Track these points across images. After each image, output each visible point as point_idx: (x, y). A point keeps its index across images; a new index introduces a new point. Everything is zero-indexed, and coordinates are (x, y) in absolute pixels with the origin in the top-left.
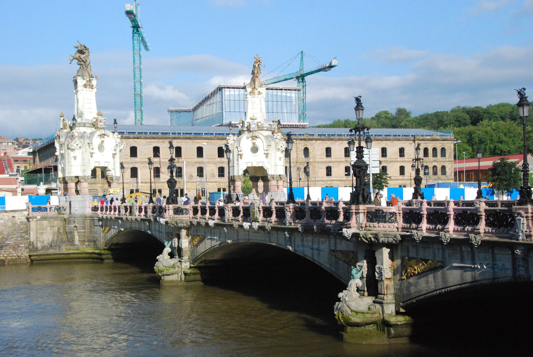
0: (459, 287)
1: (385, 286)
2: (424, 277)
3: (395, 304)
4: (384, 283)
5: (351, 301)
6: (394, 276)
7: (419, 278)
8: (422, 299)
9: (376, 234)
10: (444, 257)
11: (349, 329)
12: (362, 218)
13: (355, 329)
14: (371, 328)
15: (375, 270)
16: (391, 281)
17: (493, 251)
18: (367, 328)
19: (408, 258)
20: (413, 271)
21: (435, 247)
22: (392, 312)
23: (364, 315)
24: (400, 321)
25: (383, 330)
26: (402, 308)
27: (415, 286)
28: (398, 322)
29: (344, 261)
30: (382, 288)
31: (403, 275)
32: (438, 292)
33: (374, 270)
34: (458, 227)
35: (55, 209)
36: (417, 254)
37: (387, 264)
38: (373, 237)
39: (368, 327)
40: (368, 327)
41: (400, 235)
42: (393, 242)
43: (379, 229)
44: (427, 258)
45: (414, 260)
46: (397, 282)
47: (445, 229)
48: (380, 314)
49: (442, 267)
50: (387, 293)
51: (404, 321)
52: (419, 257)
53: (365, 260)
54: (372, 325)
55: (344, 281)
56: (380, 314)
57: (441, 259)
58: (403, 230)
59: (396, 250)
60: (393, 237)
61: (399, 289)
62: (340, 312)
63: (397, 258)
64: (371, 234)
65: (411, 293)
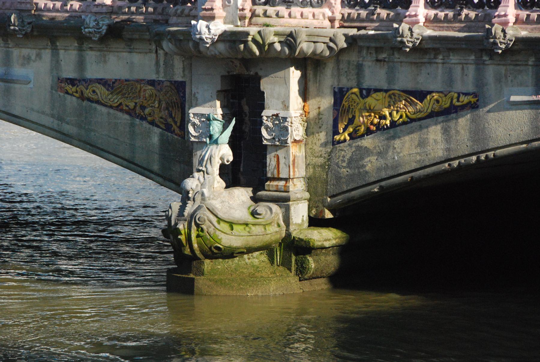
0: (526, 148)
1: (291, 159)
2: (412, 132)
3: (309, 200)
4: (288, 152)
5: (213, 199)
6: (306, 135)
7: (394, 137)
8: (405, 184)
9: (291, 35)
10: (480, 82)
11: (208, 264)
13: (221, 264)
14: (257, 260)
15: (261, 123)
16: (300, 146)
18: (247, 260)
19: (361, 90)
20: (376, 121)
21: (453, 61)
22: (303, 220)
23: (247, 229)
24: (329, 240)
25: (286, 264)
26: (329, 210)
27: (381, 154)
28: (326, 240)
30: (282, 165)
31: (341, 131)
32: (455, 164)
34: (528, 13)
36: (391, 79)
37: (296, 108)
38: (280, 42)
39: (249, 259)
40: (249, 259)
41: (345, 35)
42: (324, 54)
43: (293, 21)
44: (424, 88)
45: (380, 95)
46: (317, 148)
47: (407, 19)
48: (279, 225)
49: (474, 106)
50: (294, 175)
51: (335, 239)
52: (396, 88)
53: (218, 100)
54: (257, 253)
56: (279, 225)
57: (471, 88)
58: (346, 24)
59: (315, 75)
60: (327, 40)
61: (322, 166)
62: (193, 224)
63: (320, 93)
64: (277, 34)
65: (367, 172)
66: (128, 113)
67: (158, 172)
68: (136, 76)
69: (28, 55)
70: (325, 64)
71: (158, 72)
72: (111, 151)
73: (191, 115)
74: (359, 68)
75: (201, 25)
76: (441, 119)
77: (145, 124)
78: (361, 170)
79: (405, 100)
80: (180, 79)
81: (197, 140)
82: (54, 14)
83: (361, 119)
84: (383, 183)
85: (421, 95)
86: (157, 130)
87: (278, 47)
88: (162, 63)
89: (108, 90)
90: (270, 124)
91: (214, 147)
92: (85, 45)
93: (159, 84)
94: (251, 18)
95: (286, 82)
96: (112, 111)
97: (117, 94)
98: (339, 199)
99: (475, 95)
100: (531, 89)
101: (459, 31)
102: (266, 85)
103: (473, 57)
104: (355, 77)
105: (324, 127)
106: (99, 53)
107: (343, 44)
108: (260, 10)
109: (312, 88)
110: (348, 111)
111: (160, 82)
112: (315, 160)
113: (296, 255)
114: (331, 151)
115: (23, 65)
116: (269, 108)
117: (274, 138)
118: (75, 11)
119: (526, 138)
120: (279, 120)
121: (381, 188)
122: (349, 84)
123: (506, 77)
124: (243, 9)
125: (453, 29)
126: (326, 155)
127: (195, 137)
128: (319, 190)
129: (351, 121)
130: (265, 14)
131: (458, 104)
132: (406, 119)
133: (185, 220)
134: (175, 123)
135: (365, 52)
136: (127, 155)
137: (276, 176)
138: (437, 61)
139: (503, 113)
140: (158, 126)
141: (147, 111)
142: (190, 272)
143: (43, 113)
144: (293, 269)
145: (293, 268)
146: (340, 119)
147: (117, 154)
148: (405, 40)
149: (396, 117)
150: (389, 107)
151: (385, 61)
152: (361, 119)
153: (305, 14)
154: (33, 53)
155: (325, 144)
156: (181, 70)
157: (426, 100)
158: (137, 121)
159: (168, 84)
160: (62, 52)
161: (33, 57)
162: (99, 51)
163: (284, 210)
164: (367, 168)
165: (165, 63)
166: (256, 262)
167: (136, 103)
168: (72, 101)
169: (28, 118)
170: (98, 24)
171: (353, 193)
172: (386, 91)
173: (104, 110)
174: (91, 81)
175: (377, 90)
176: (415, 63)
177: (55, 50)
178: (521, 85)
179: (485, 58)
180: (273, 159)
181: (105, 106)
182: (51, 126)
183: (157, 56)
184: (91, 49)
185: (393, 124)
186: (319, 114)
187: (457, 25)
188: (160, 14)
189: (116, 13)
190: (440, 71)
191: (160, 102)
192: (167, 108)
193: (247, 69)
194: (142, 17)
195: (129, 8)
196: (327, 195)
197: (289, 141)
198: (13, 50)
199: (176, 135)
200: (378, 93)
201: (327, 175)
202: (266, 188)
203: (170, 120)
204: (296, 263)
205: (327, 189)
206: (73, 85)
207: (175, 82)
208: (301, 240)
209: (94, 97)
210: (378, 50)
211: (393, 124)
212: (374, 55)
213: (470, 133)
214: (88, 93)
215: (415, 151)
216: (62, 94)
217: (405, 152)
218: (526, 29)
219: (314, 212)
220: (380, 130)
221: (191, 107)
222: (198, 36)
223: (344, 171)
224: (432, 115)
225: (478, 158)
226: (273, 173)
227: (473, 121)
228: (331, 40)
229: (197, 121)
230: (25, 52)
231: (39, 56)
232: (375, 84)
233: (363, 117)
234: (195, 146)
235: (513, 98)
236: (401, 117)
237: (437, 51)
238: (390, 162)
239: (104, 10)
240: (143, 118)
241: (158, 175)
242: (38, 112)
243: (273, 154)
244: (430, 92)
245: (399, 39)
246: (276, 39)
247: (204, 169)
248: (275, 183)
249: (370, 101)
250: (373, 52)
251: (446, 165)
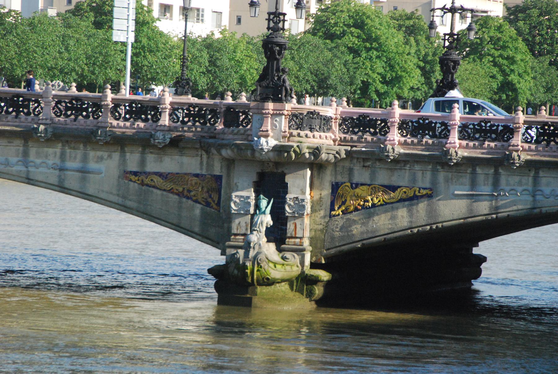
4: (303, 221)
8: (379, 242)
9: (317, 148)
11: (259, 289)
12: (284, 123)
17: (537, 173)
19: (352, 184)
20: (362, 203)
25: (300, 291)
31: (336, 209)
32: (415, 230)
33: (284, 202)
35: (67, 108)
41: (345, 150)
45: (365, 188)
46: (318, 219)
48: (298, 266)
56: (298, 266)
57: (428, 185)
58: (342, 144)
60: (335, 153)
61: (321, 231)
64: (308, 148)
65: (353, 235)
66: (177, 194)
67: (198, 233)
68: (184, 171)
69: (102, 156)
70: (326, 167)
71: (201, 169)
72: (162, 218)
73: (234, 196)
74: (351, 170)
75: (263, 140)
76: (407, 203)
77: (190, 202)
78: (349, 233)
79: (382, 191)
80: (218, 174)
81: (236, 212)
82: (124, 130)
83: (352, 202)
84: (365, 242)
85: (394, 188)
86: (199, 206)
87: (307, 155)
88: (205, 163)
89: (163, 179)
90: (292, 203)
91: (263, 216)
92: (147, 150)
93: (202, 176)
94: (289, 138)
95: (304, 177)
96: (165, 193)
97: (170, 182)
98: (333, 251)
99: (431, 189)
100: (468, 187)
101: (422, 151)
102: (289, 179)
103: (430, 167)
104: (347, 176)
105: (324, 207)
106: (156, 156)
107: (343, 156)
108: (295, 132)
109: (316, 182)
110: (342, 197)
111: (202, 175)
112: (316, 227)
113: (307, 285)
114: (328, 221)
115: (97, 162)
116: (291, 193)
117: (294, 212)
118: (141, 128)
119: (464, 216)
120: (299, 201)
121: (363, 244)
122: (343, 180)
123: (452, 179)
124: (285, 132)
125: (417, 149)
126: (325, 224)
127: (235, 210)
128: (319, 245)
129: (344, 203)
130: (299, 135)
131: (419, 194)
132: (383, 203)
133: (250, 261)
134: (214, 201)
135: (355, 161)
136: (175, 222)
137: (294, 236)
138: (406, 168)
139: (449, 201)
140: (200, 203)
141: (192, 193)
142: (247, 293)
143: (111, 193)
144: (305, 294)
145: (305, 293)
146: (335, 202)
147: (167, 220)
148: (390, 154)
149: (376, 201)
150: (371, 195)
151: (369, 167)
152: (352, 202)
153: (301, 135)
154: (105, 155)
155: (324, 217)
156: (219, 168)
157: (397, 192)
158: (184, 200)
159: (210, 176)
160: (128, 155)
161: (105, 157)
162: (157, 154)
163: (300, 257)
164: (354, 232)
165: (208, 163)
166: (283, 288)
167: (184, 189)
168: (134, 186)
169: (100, 197)
170: (164, 137)
171: (343, 248)
172: (369, 185)
173: (159, 192)
174: (150, 173)
175: (362, 185)
176: (390, 169)
177: (123, 152)
178: (462, 184)
179: (438, 167)
180: (292, 225)
181: (160, 189)
182: (116, 202)
183: (201, 159)
184: (151, 153)
185: (374, 205)
186: (321, 198)
187: (420, 147)
188: (206, 132)
189: (172, 131)
190: (407, 174)
191: (202, 188)
192: (208, 192)
193: (277, 169)
194: (191, 134)
195: (183, 128)
196: (324, 248)
197: (305, 214)
198: (90, 152)
199: (214, 209)
200: (364, 187)
201: (325, 236)
202: (286, 243)
203: (209, 200)
204: (307, 291)
205: (324, 245)
206: (136, 176)
207: (215, 175)
208: (313, 276)
209: (153, 184)
210: (365, 160)
211: (374, 205)
212: (362, 163)
213: (426, 212)
214: (147, 181)
215: (388, 222)
216: (126, 181)
217: (381, 223)
218: (466, 152)
219: (314, 259)
220: (364, 209)
221: (233, 191)
222: (260, 147)
223: (337, 234)
224: (401, 200)
225: (431, 228)
226: (291, 234)
227: (428, 205)
228: (337, 153)
229: (238, 201)
230: (99, 153)
231: (110, 157)
232: (362, 181)
233: (353, 200)
234: (234, 216)
235: (456, 192)
236: (379, 201)
237: (406, 162)
238: (370, 229)
239: (166, 128)
240: (188, 198)
241: (197, 234)
242: (107, 192)
243: (292, 222)
244: (399, 187)
245: (386, 154)
246: (307, 151)
247: (258, 229)
248: (293, 240)
249: (358, 191)
250: (361, 160)
251: (409, 231)
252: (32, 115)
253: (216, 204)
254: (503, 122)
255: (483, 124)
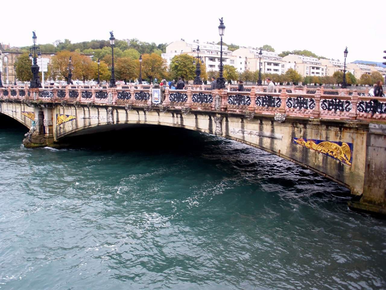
29: (29, 117)
36: (64, 113)
55: (28, 128)
252: (276, 106)
253: (349, 162)
254: (346, 99)
255: (334, 101)
